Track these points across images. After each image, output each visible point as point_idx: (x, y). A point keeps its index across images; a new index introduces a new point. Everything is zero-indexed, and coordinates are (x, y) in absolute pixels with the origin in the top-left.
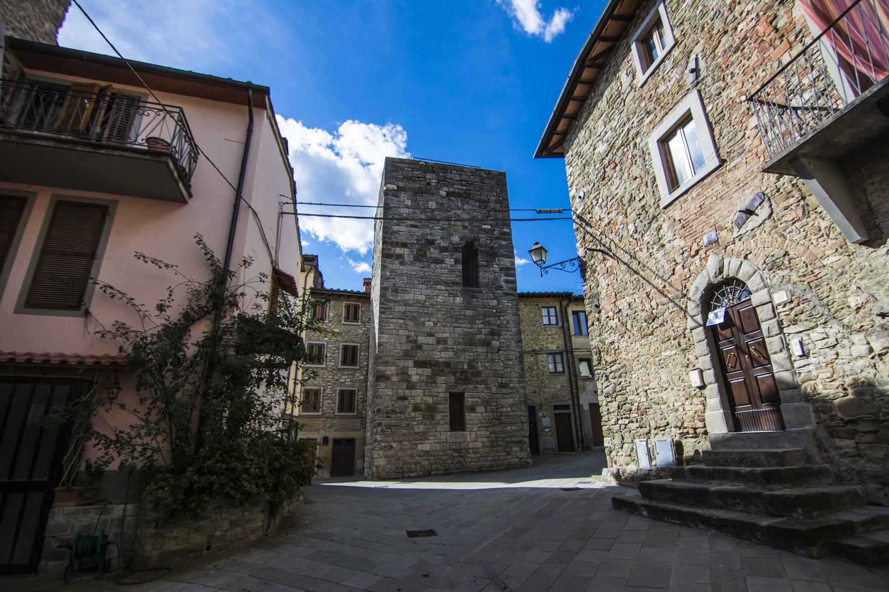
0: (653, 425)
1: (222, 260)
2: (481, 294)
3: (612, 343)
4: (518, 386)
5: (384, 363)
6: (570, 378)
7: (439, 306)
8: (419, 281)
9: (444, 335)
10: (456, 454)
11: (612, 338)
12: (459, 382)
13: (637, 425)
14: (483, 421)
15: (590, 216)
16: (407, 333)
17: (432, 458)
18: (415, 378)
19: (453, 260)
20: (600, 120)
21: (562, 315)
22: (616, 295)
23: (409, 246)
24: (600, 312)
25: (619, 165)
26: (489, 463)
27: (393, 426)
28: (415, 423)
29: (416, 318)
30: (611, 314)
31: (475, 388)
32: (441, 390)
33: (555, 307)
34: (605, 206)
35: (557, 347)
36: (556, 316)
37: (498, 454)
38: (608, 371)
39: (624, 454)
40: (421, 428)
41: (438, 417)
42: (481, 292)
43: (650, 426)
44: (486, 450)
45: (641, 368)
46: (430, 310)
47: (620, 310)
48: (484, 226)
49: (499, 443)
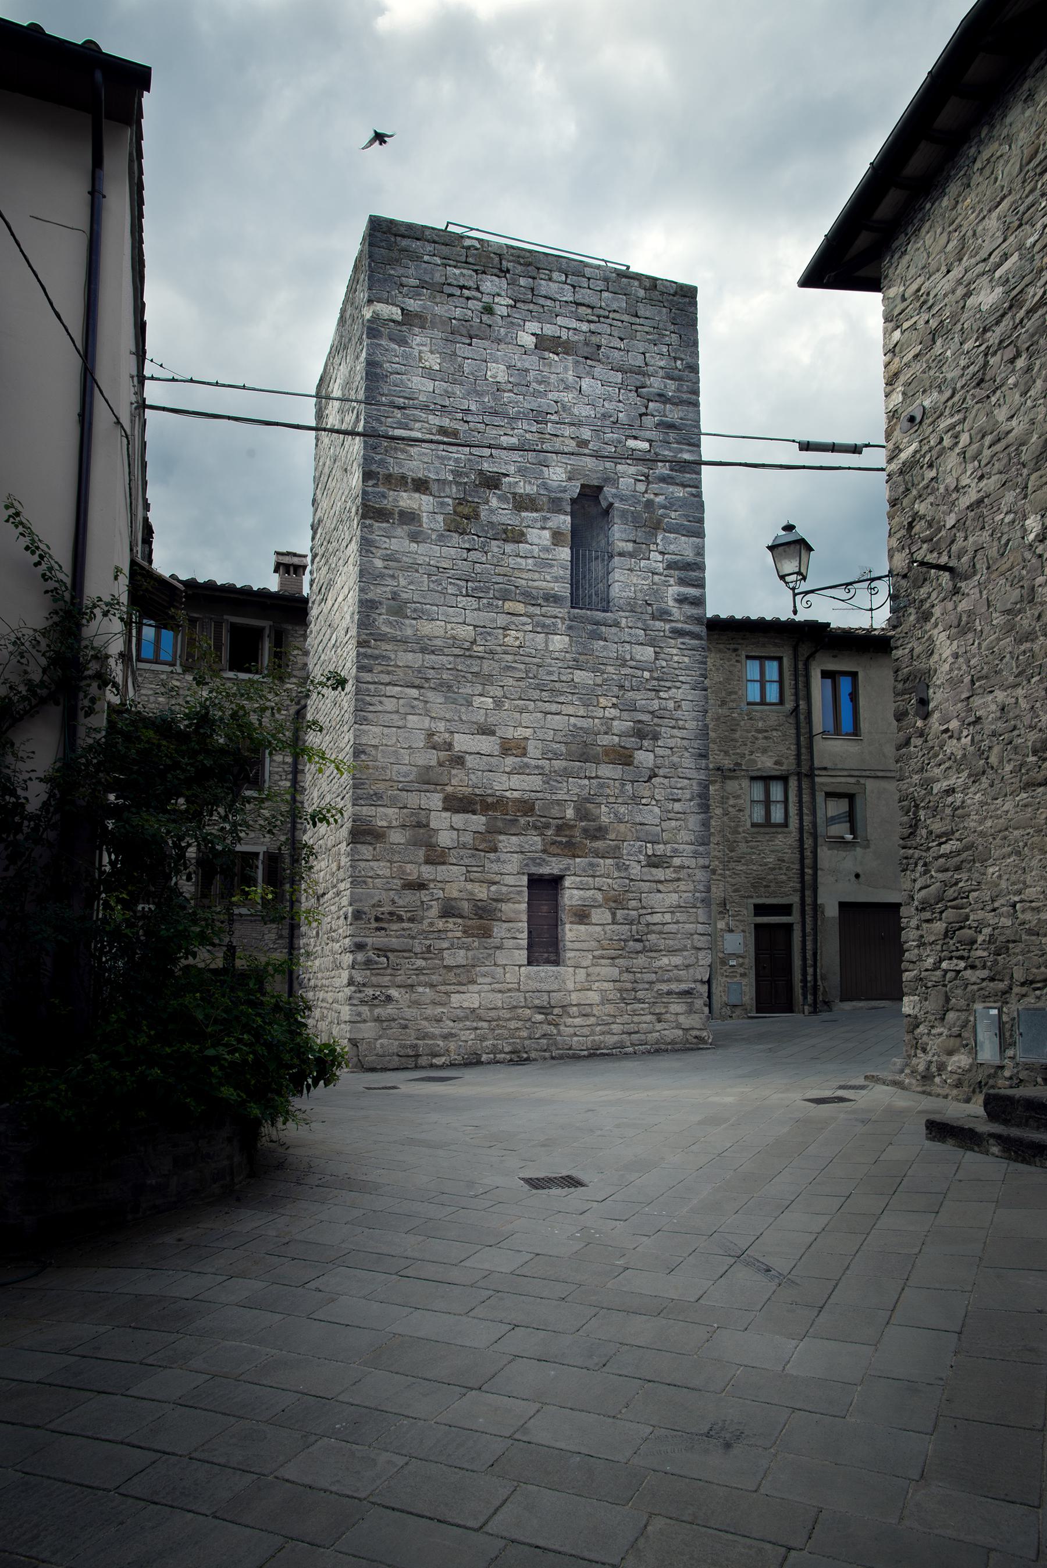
0: (1019, 975)
1: (67, 567)
2: (614, 630)
3: (950, 791)
4: (692, 863)
5: (370, 797)
6: (801, 840)
7: (509, 658)
8: (460, 588)
9: (521, 733)
10: (540, 1017)
11: (952, 781)
12: (553, 849)
13: (985, 973)
14: (605, 943)
15: (932, 474)
16: (426, 722)
17: (485, 1025)
18: (445, 839)
19: (547, 534)
20: (994, 215)
21: (796, 680)
22: (973, 682)
23: (434, 487)
24: (926, 716)
25: (1024, 356)
26: (616, 1038)
27: (393, 951)
28: (445, 945)
29: (450, 687)
30: (954, 724)
31: (591, 865)
32: (509, 868)
33: (779, 659)
34: (974, 458)
35: (776, 763)
36: (781, 682)
37: (636, 1019)
38: (932, 853)
39: (946, 1032)
40: (460, 957)
41: (499, 930)
42: (617, 624)
43: (1012, 977)
44: (610, 1009)
45: (1010, 855)
46: (487, 666)
47: (978, 719)
48: (631, 443)
49: (640, 994)
